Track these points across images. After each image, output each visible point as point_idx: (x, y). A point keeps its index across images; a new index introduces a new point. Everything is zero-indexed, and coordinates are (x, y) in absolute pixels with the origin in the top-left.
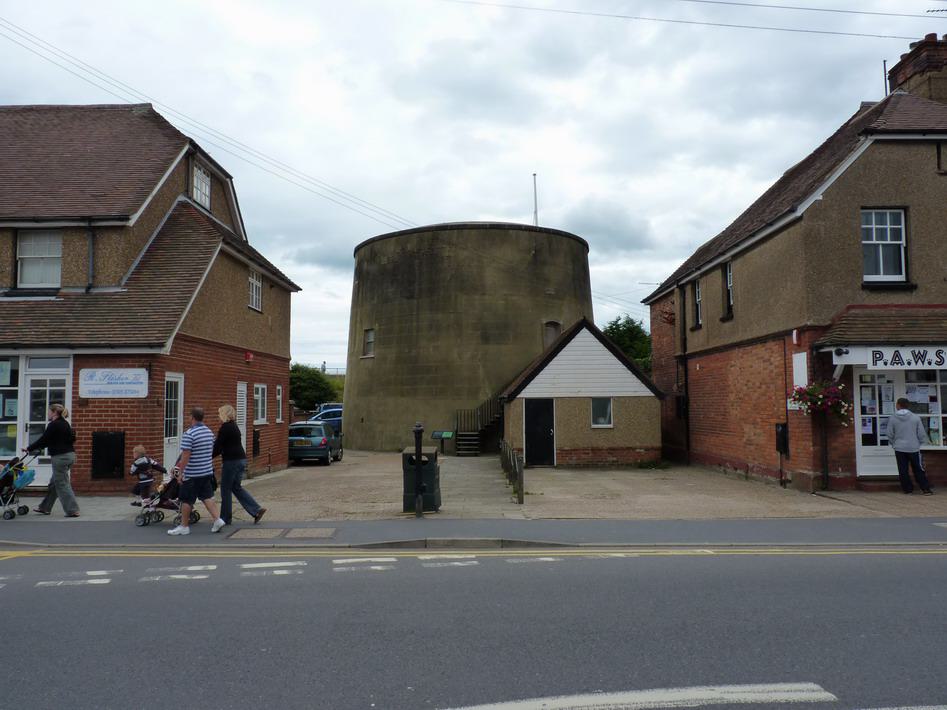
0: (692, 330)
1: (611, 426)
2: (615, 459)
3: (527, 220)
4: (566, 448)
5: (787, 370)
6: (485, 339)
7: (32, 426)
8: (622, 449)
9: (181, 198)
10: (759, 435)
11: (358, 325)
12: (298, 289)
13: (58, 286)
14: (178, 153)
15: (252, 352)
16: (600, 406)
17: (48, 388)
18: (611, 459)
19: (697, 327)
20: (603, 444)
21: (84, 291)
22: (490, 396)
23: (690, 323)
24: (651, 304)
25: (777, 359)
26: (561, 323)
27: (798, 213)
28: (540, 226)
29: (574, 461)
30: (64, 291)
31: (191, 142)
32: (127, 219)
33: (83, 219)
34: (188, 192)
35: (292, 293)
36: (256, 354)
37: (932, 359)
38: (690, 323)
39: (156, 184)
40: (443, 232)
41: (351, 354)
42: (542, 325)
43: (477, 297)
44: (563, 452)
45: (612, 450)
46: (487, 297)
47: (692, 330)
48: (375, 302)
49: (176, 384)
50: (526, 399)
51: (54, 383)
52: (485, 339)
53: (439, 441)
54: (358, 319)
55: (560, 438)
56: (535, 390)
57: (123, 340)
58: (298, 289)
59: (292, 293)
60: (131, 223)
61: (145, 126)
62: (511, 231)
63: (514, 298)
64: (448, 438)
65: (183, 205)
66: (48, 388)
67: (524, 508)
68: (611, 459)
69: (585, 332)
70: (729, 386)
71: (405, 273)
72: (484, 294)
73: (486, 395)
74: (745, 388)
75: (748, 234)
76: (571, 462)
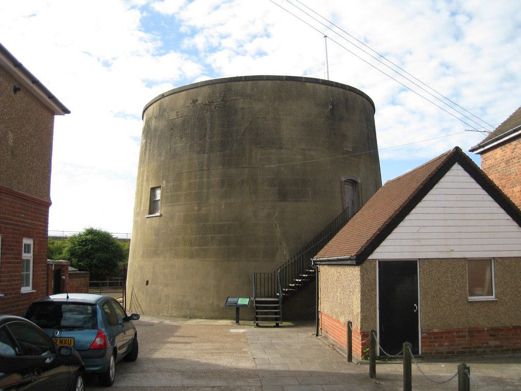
1: (492, 298)
2: (498, 343)
3: (322, 76)
4: (436, 331)
6: (283, 196)
8: (508, 329)
11: (145, 183)
12: (66, 111)
16: (476, 270)
18: (493, 343)
20: (483, 323)
22: (288, 258)
26: (359, 181)
28: (330, 80)
29: (445, 346)
35: (56, 116)
37: (2, 274)
40: (236, 83)
42: (341, 181)
43: (273, 151)
44: (432, 336)
45: (494, 332)
46: (282, 151)
48: (163, 158)
52: (283, 196)
53: (235, 308)
54: (145, 178)
55: (427, 316)
58: (66, 111)
59: (56, 116)
61: (91, 232)
62: (308, 84)
63: (312, 153)
64: (245, 305)
68: (493, 343)
72: (281, 148)
73: (284, 255)
76: (441, 349)
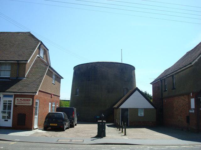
0: (164, 91)
3: (120, 62)
5: (189, 103)
7: (3, 112)
9: (38, 55)
10: (182, 119)
13: (9, 77)
14: (37, 45)
15: (53, 94)
17: (7, 102)
19: (165, 91)
21: (16, 78)
23: (163, 89)
24: (153, 84)
25: (187, 100)
27: (192, 64)
30: (11, 78)
31: (42, 43)
32: (27, 61)
33: (17, 61)
34: (39, 54)
36: (54, 95)
38: (163, 89)
39: (33, 52)
41: (190, 101)
47: (164, 91)
49: (37, 102)
50: (122, 108)
51: (9, 101)
56: (123, 106)
57: (27, 91)
60: (28, 62)
65: (38, 57)
66: (7, 102)
67: (125, 137)
69: (137, 91)
70: (174, 106)
71: (86, 74)
74: (178, 107)
75: (179, 68)
